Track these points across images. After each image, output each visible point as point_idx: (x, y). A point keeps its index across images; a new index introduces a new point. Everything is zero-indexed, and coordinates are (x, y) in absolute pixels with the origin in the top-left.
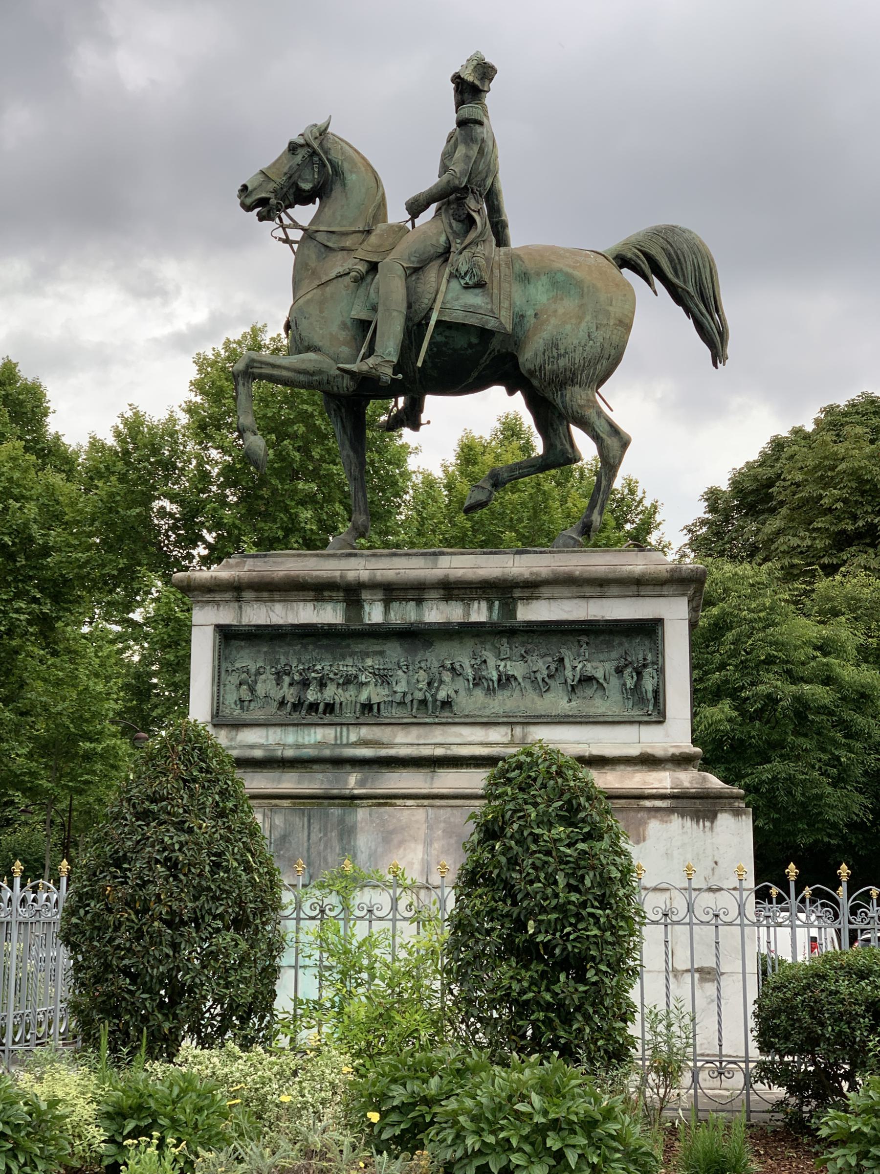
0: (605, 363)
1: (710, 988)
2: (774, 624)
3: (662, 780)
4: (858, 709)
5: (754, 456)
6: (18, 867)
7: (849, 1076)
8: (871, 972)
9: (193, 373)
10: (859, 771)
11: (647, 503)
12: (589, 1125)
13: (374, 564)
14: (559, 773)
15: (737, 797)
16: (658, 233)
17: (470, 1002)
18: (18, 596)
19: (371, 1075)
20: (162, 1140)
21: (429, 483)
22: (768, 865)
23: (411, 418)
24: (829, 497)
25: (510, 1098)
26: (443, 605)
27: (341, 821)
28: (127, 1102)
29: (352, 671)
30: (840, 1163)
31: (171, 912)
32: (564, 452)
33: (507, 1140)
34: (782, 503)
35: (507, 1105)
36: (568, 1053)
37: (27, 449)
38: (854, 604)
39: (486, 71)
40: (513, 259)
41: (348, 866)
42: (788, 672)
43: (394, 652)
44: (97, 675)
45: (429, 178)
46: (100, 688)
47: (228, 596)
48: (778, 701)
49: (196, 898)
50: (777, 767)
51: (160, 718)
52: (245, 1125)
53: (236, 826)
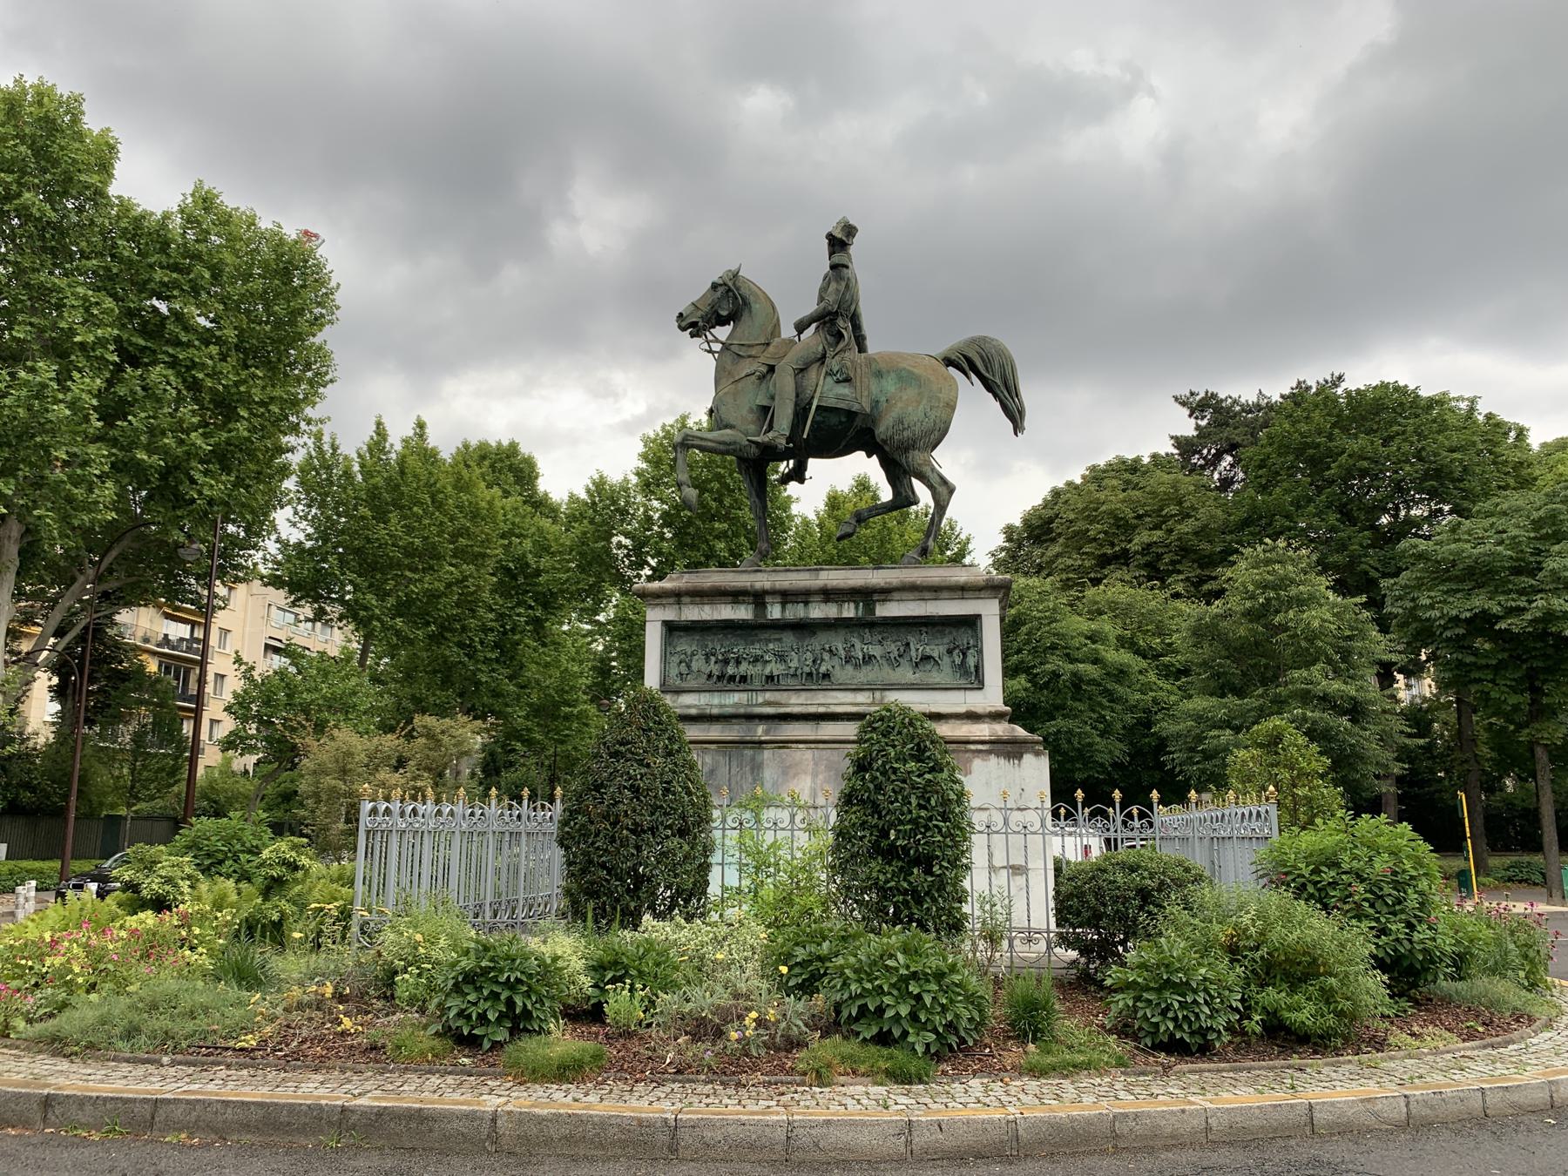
0: (937, 434)
1: (1020, 881)
2: (1056, 621)
3: (983, 730)
4: (1119, 682)
5: (1038, 501)
6: (526, 792)
7: (1123, 943)
8: (1139, 867)
9: (641, 448)
10: (1119, 726)
11: (963, 537)
12: (939, 976)
13: (774, 577)
14: (911, 724)
15: (1037, 743)
16: (973, 341)
17: (848, 888)
18: (519, 604)
19: (780, 940)
20: (632, 985)
21: (806, 523)
22: (1061, 791)
23: (798, 475)
24: (1094, 530)
25: (881, 957)
26: (823, 606)
27: (753, 759)
28: (607, 959)
29: (759, 652)
30: (1121, 1004)
31: (635, 824)
32: (907, 497)
33: (880, 987)
34: (1060, 535)
35: (879, 962)
36: (922, 926)
37: (525, 502)
38: (1113, 606)
39: (850, 230)
40: (870, 361)
41: (759, 791)
42: (1067, 655)
43: (789, 639)
44: (573, 660)
45: (810, 307)
46: (576, 669)
47: (671, 600)
48: (1059, 676)
49: (652, 814)
50: (1059, 723)
51: (618, 691)
52: (691, 975)
53: (681, 762)
